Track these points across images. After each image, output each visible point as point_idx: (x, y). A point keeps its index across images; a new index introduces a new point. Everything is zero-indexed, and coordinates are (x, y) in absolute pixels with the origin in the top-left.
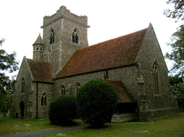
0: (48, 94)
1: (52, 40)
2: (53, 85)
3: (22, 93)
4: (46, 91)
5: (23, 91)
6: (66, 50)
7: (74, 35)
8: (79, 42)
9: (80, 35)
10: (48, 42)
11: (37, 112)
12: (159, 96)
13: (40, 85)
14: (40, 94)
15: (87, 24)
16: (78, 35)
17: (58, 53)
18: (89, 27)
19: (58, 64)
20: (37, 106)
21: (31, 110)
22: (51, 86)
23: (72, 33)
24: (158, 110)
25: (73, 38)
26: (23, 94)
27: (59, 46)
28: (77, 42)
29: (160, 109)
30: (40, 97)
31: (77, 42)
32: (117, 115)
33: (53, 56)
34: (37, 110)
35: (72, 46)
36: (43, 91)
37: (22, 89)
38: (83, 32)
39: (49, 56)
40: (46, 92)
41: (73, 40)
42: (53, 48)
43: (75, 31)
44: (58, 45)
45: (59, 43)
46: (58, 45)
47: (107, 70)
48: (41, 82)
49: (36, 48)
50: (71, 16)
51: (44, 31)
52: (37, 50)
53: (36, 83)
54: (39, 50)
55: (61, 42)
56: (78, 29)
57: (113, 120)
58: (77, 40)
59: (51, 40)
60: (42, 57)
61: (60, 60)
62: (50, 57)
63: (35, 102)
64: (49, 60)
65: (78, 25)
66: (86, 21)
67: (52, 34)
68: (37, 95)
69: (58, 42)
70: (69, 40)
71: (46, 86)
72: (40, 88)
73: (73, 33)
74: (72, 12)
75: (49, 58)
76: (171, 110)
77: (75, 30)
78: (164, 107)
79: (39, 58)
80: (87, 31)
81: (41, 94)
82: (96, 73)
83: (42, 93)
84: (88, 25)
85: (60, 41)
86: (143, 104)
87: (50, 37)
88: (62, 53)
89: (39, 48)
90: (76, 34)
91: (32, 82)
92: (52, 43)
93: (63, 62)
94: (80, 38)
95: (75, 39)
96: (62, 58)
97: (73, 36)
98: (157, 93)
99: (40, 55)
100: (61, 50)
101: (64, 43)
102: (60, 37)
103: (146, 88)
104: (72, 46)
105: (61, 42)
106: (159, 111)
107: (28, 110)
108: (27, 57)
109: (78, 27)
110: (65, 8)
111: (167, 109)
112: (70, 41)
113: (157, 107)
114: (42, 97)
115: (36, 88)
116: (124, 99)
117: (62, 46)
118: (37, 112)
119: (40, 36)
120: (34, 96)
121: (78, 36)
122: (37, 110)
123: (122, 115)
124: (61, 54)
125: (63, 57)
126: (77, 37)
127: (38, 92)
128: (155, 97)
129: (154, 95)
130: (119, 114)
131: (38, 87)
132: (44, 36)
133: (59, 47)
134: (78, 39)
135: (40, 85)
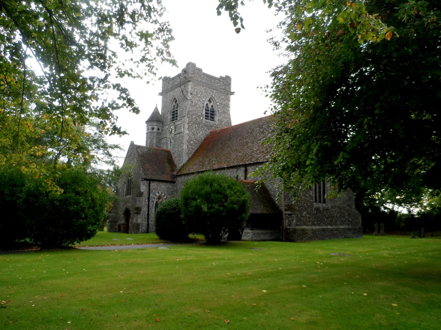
0: (165, 197)
1: (175, 116)
2: (173, 184)
3: (128, 195)
4: (162, 193)
5: (128, 193)
6: (195, 133)
7: (208, 107)
8: (217, 118)
9: (219, 107)
10: (169, 118)
11: (148, 224)
12: (326, 206)
13: (153, 185)
14: (154, 198)
15: (230, 89)
16: (214, 107)
17: (182, 137)
18: (233, 93)
19: (182, 153)
20: (148, 215)
21: (139, 221)
22: (169, 185)
23: (205, 105)
24: (322, 227)
25: (206, 113)
26: (129, 196)
27: (184, 125)
28: (213, 118)
29: (325, 227)
30: (153, 202)
31: (212, 119)
32: (249, 230)
33: (176, 142)
34: (148, 221)
35: (204, 126)
36: (158, 193)
37: (128, 190)
38: (224, 103)
39: (169, 141)
40: (163, 195)
41: (206, 116)
42: (175, 128)
43: (211, 102)
44: (182, 125)
45: (184, 121)
46: (182, 125)
47: (246, 166)
48: (154, 180)
49: (151, 126)
50: (204, 78)
51: (163, 102)
52: (152, 131)
53: (148, 182)
54: (155, 130)
55: (186, 120)
56: (215, 98)
57: (243, 238)
58: (213, 115)
59: (173, 115)
60: (159, 141)
61: (185, 147)
62: (171, 142)
63: (145, 209)
64: (169, 146)
65: (215, 92)
66: (229, 84)
67: (174, 106)
68: (149, 199)
69: (183, 120)
70: (199, 115)
71: (163, 186)
72: (154, 189)
73: (207, 104)
74: (204, 71)
75: (169, 143)
76: (349, 229)
77: (210, 100)
78: (336, 225)
79: (155, 142)
80: (229, 101)
81: (155, 197)
82: (231, 170)
83: (156, 195)
84: (232, 91)
85: (185, 118)
86: (288, 218)
87: (172, 110)
88: (188, 137)
89: (156, 127)
90: (212, 106)
91: (142, 180)
92: (174, 120)
93: (189, 150)
94: (217, 112)
95: (210, 114)
96: (187, 144)
97: (206, 110)
98: (322, 201)
99: (156, 139)
100: (187, 132)
101: (191, 121)
102: (185, 113)
103: (300, 194)
104: (204, 126)
105: (186, 120)
106: (324, 230)
107: (134, 221)
108: (136, 143)
109: (215, 94)
110: (193, 65)
111: (342, 227)
112: (202, 118)
113: (319, 224)
114: (157, 201)
115: (148, 189)
116: (256, 208)
117: (189, 126)
118: (148, 224)
119: (156, 109)
120: (144, 199)
121: (215, 110)
122: (148, 221)
123: (256, 231)
124: (186, 138)
125: (189, 142)
126: (213, 112)
127: (151, 195)
128: (317, 209)
129: (315, 205)
130: (252, 229)
131: (151, 187)
132: (163, 108)
133: (184, 127)
134: (215, 113)
135: (153, 184)
